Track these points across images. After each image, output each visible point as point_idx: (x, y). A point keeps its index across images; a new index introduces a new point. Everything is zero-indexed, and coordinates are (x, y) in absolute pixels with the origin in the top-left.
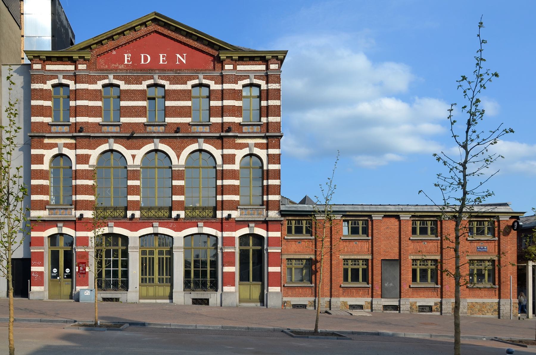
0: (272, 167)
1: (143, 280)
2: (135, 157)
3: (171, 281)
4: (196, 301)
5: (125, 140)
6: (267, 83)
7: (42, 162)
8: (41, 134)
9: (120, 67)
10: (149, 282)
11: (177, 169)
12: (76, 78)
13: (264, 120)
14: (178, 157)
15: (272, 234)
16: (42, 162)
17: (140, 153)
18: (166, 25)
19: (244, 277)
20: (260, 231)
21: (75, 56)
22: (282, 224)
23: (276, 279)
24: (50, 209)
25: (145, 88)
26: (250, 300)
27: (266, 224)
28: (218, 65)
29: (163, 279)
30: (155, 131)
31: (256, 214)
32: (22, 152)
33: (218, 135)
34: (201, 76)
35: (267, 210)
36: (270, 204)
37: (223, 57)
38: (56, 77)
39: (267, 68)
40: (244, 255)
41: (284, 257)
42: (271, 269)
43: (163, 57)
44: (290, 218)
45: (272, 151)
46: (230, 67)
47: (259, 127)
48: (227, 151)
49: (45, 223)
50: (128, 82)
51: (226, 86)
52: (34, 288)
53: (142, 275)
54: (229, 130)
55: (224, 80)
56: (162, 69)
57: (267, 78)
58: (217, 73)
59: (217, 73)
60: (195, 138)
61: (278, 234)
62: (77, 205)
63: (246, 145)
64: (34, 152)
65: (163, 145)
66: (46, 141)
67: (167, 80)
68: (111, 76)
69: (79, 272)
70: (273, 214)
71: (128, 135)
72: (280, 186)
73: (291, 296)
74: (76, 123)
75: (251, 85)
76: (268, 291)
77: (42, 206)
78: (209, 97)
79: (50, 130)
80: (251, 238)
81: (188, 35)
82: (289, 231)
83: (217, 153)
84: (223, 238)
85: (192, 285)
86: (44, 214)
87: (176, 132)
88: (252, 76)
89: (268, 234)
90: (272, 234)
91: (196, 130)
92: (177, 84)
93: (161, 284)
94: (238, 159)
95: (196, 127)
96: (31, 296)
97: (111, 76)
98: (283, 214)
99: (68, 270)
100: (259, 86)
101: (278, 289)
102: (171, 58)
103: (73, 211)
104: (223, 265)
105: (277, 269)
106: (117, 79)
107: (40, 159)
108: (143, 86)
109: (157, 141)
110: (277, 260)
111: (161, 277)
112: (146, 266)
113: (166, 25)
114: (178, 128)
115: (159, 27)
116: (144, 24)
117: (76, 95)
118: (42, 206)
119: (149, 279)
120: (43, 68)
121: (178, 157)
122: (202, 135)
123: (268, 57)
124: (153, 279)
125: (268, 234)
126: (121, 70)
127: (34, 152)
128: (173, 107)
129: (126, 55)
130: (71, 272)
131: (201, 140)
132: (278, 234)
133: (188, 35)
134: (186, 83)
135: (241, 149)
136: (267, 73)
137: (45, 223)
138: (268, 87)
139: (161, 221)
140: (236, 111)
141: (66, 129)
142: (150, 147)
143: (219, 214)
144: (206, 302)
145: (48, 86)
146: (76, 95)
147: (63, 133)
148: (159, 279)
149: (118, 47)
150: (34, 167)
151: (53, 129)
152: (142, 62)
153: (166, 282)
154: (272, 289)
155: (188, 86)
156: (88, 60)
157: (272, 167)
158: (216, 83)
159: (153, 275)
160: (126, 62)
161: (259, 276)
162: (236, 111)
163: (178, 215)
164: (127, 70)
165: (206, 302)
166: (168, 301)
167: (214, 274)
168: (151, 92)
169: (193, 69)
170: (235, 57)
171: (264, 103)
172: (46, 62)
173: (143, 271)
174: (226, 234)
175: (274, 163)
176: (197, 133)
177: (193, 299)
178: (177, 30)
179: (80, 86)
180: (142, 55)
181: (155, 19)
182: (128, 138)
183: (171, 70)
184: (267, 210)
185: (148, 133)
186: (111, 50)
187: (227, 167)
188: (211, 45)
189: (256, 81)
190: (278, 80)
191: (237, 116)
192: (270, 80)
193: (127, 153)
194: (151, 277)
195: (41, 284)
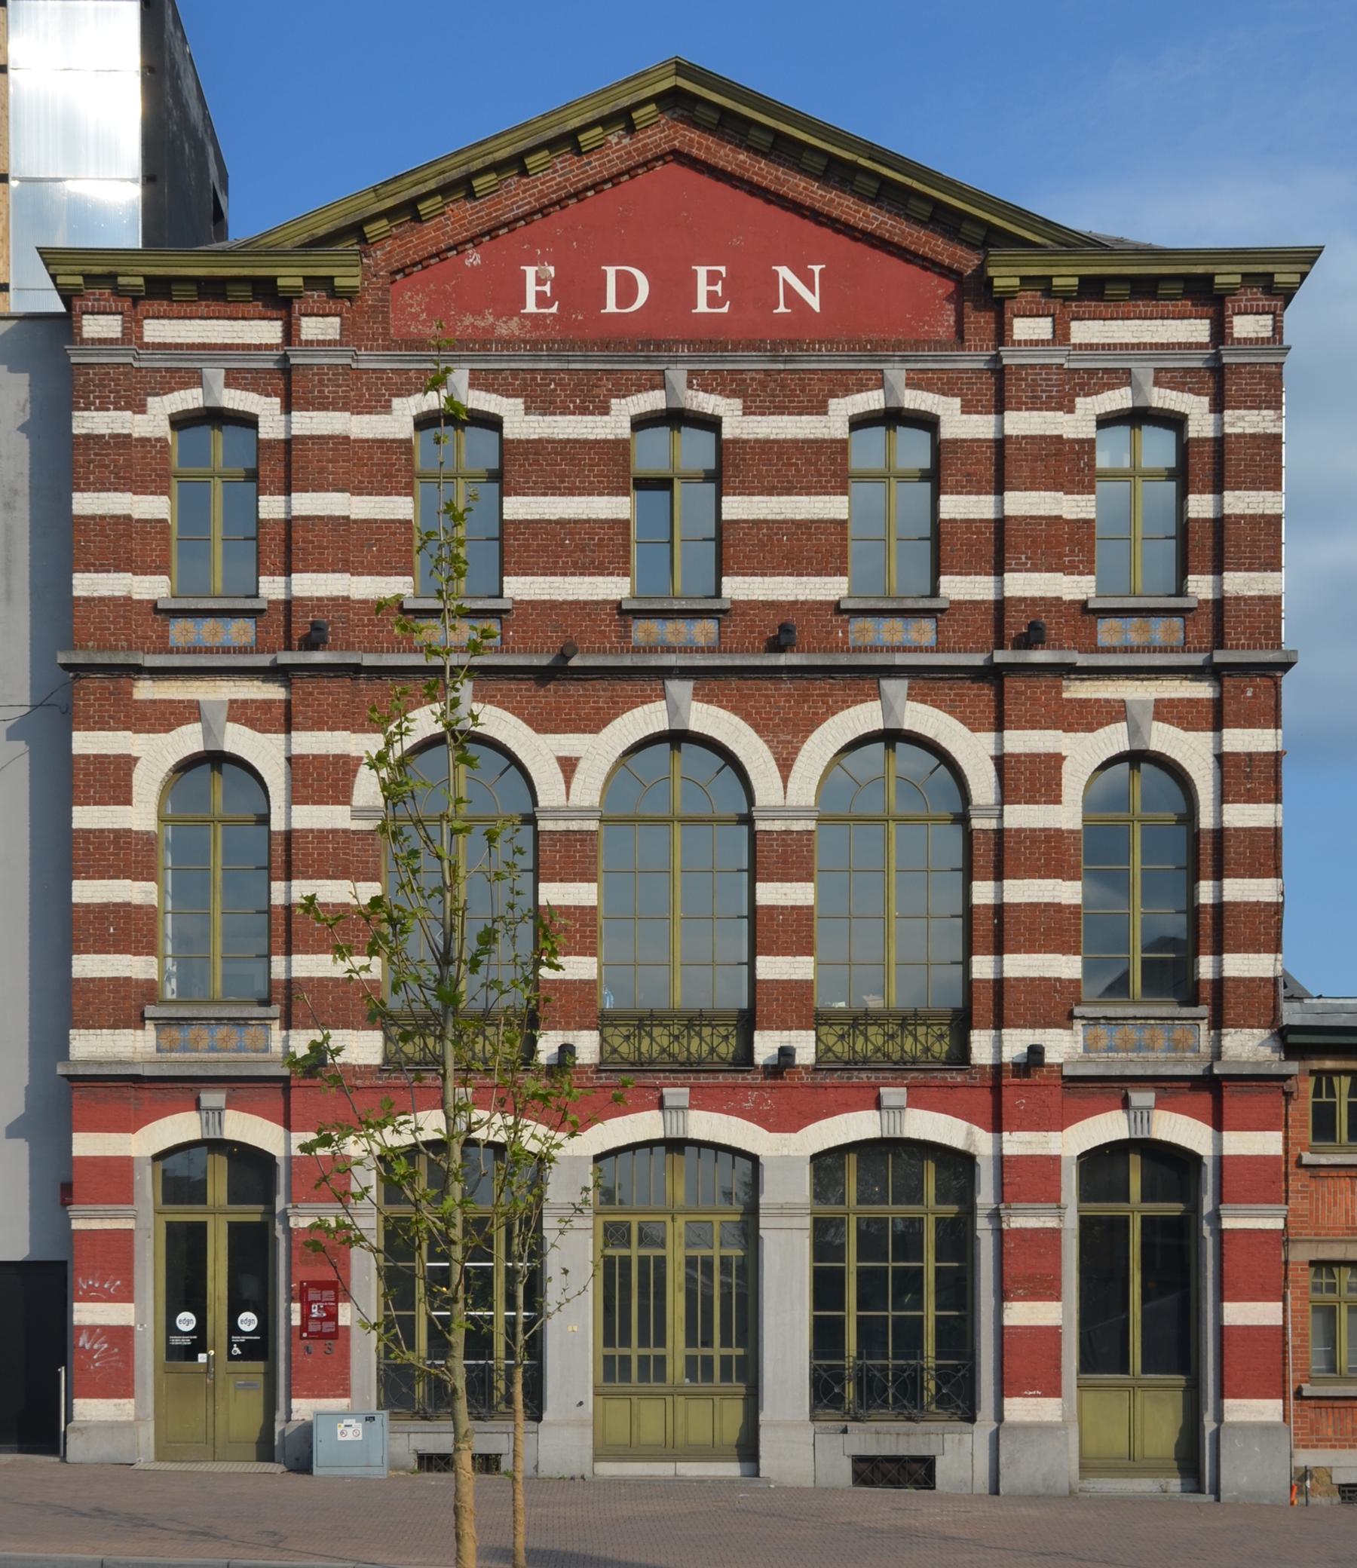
0: (1241, 816)
1: (612, 1370)
2: (571, 768)
3: (748, 1373)
4: (871, 1471)
5: (525, 688)
6: (1218, 406)
7: (123, 796)
8: (119, 659)
9: (503, 330)
10: (643, 1376)
11: (778, 826)
12: (290, 384)
13: (1201, 587)
14: (785, 766)
15: (1240, 1143)
16: (123, 796)
17: (600, 750)
18: (729, 126)
19: (1102, 1351)
20: (1182, 1130)
21: (289, 278)
22: (1288, 1095)
23: (1262, 1363)
24: (163, 1023)
25: (624, 431)
26: (1131, 1465)
27: (1213, 1093)
28: (980, 321)
29: (626, 1360)
30: (672, 640)
31: (1161, 1043)
32: (21, 746)
33: (978, 660)
34: (895, 373)
35: (1218, 1023)
36: (1230, 998)
37: (1004, 278)
38: (193, 379)
39: (1220, 333)
40: (1100, 1240)
41: (1301, 1254)
42: (1239, 1313)
43: (713, 278)
44: (1329, 1064)
45: (1240, 740)
46: (1038, 328)
47: (1177, 622)
48: (1020, 741)
49: (132, 1094)
50: (540, 403)
51: (1021, 423)
52: (88, 1410)
53: (608, 1341)
54: (1033, 638)
55: (1011, 391)
56: (708, 339)
57: (1219, 383)
58: (973, 361)
59: (973, 361)
60: (864, 679)
61: (1268, 1143)
62: (292, 1002)
63: (1115, 712)
64: (86, 743)
65: (713, 709)
66: (145, 690)
67: (733, 394)
68: (460, 377)
69: (304, 1327)
70: (1247, 1046)
71: (544, 661)
72: (1277, 908)
73: (1340, 1442)
74: (289, 605)
75: (893, 418)
76: (1219, 1417)
77: (125, 1004)
78: (935, 478)
79: (164, 636)
80: (1135, 1161)
81: (837, 172)
82: (1323, 1126)
83: (974, 751)
84: (1002, 1161)
85: (850, 1390)
86: (130, 1046)
87: (776, 646)
88: (215, 374)
89: (1218, 1144)
90: (1240, 1143)
91: (869, 639)
92: (780, 410)
93: (702, 1386)
94: (1074, 781)
95: (869, 623)
96: (76, 1447)
97: (460, 377)
98: (1293, 1042)
99: (248, 1321)
100: (1175, 421)
101: (1269, 1410)
102: (749, 286)
103: (277, 1034)
104: (1002, 1295)
105: (1265, 1313)
106: (488, 388)
107: (113, 780)
108: (613, 423)
109: (682, 689)
110: (1263, 1267)
111: (700, 1351)
112: (628, 1296)
113: (729, 126)
114: (785, 629)
115: (694, 135)
116: (623, 119)
117: (292, 464)
118: (125, 1004)
119: (643, 1360)
120: (132, 334)
121: (785, 766)
122: (900, 659)
123: (1227, 277)
124: (661, 1361)
125: (1218, 1144)
126: (507, 343)
127: (86, 743)
128: (757, 523)
129: (531, 272)
130: (266, 1327)
131: (895, 688)
132: (1268, 1143)
133: (837, 172)
134: (821, 409)
135: (1090, 728)
136: (1217, 357)
137: (132, 1094)
138: (1220, 424)
139: (703, 1079)
140: (1063, 546)
141: (241, 631)
142: (647, 718)
143: (982, 1046)
144: (917, 1472)
145: (152, 421)
146: (292, 464)
147: (227, 650)
148: (690, 1361)
149: (491, 232)
150: (86, 817)
151: (180, 631)
152: (611, 307)
153: (726, 1376)
154: (1241, 1410)
155: (832, 422)
156: (350, 295)
157: (1241, 816)
158: (967, 409)
159: (661, 1341)
160: (531, 307)
161: (1177, 1348)
162: (1063, 546)
163: (567, 1050)
164: (535, 345)
165: (917, 1472)
166: (732, 1469)
167: (958, 1336)
168: (653, 453)
169: (855, 341)
170: (1066, 278)
171: (1201, 506)
172: (144, 307)
173: (613, 1325)
174: (1018, 1143)
175: (1251, 798)
176: (874, 649)
177: (858, 1460)
178: (783, 149)
179: (309, 423)
180: (611, 272)
181: (675, 92)
182: (542, 675)
183: (752, 345)
184: (1218, 1023)
185: (637, 650)
186: (458, 247)
187: (1021, 816)
188: (944, 219)
189: (235, 400)
190: (1267, 390)
191: (1069, 569)
192: (1231, 389)
193: (538, 750)
194: (652, 1351)
195: (119, 1386)
